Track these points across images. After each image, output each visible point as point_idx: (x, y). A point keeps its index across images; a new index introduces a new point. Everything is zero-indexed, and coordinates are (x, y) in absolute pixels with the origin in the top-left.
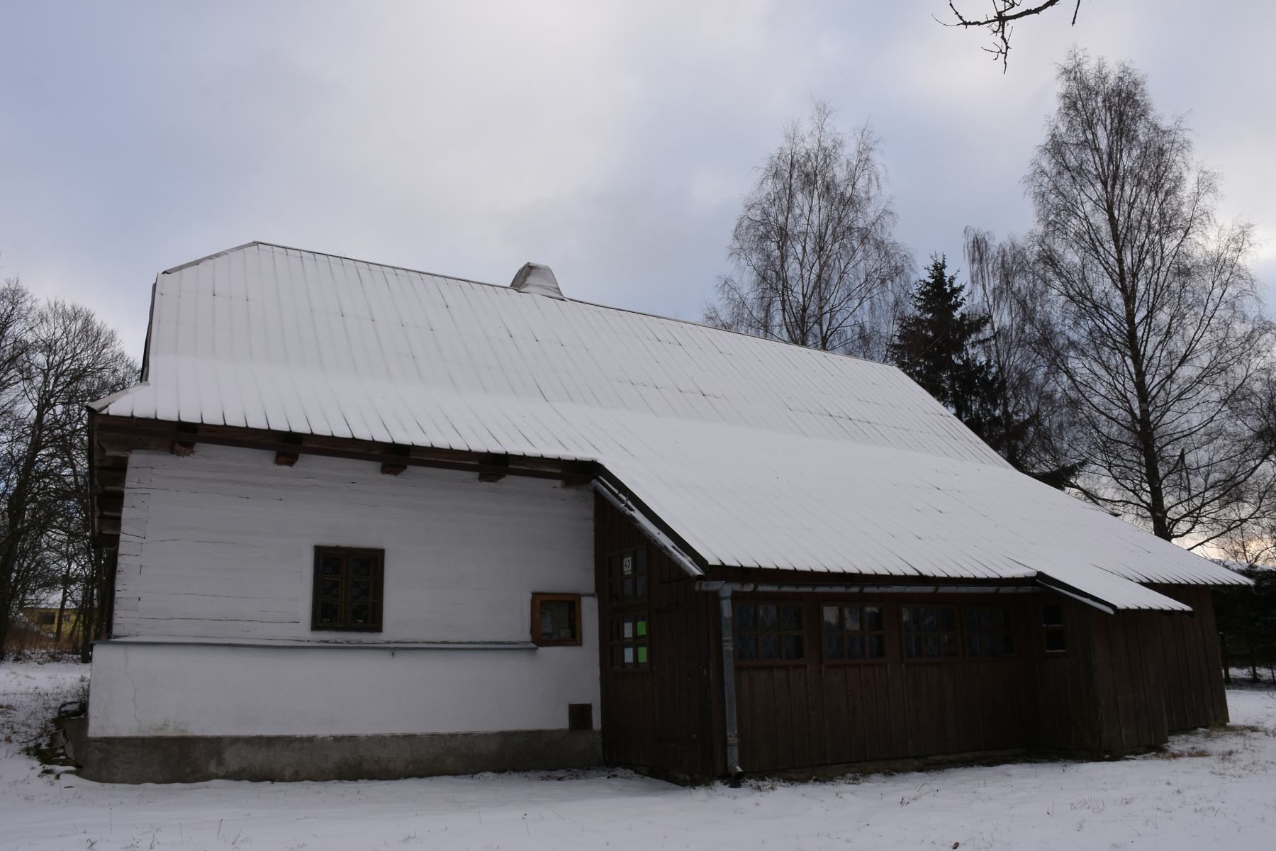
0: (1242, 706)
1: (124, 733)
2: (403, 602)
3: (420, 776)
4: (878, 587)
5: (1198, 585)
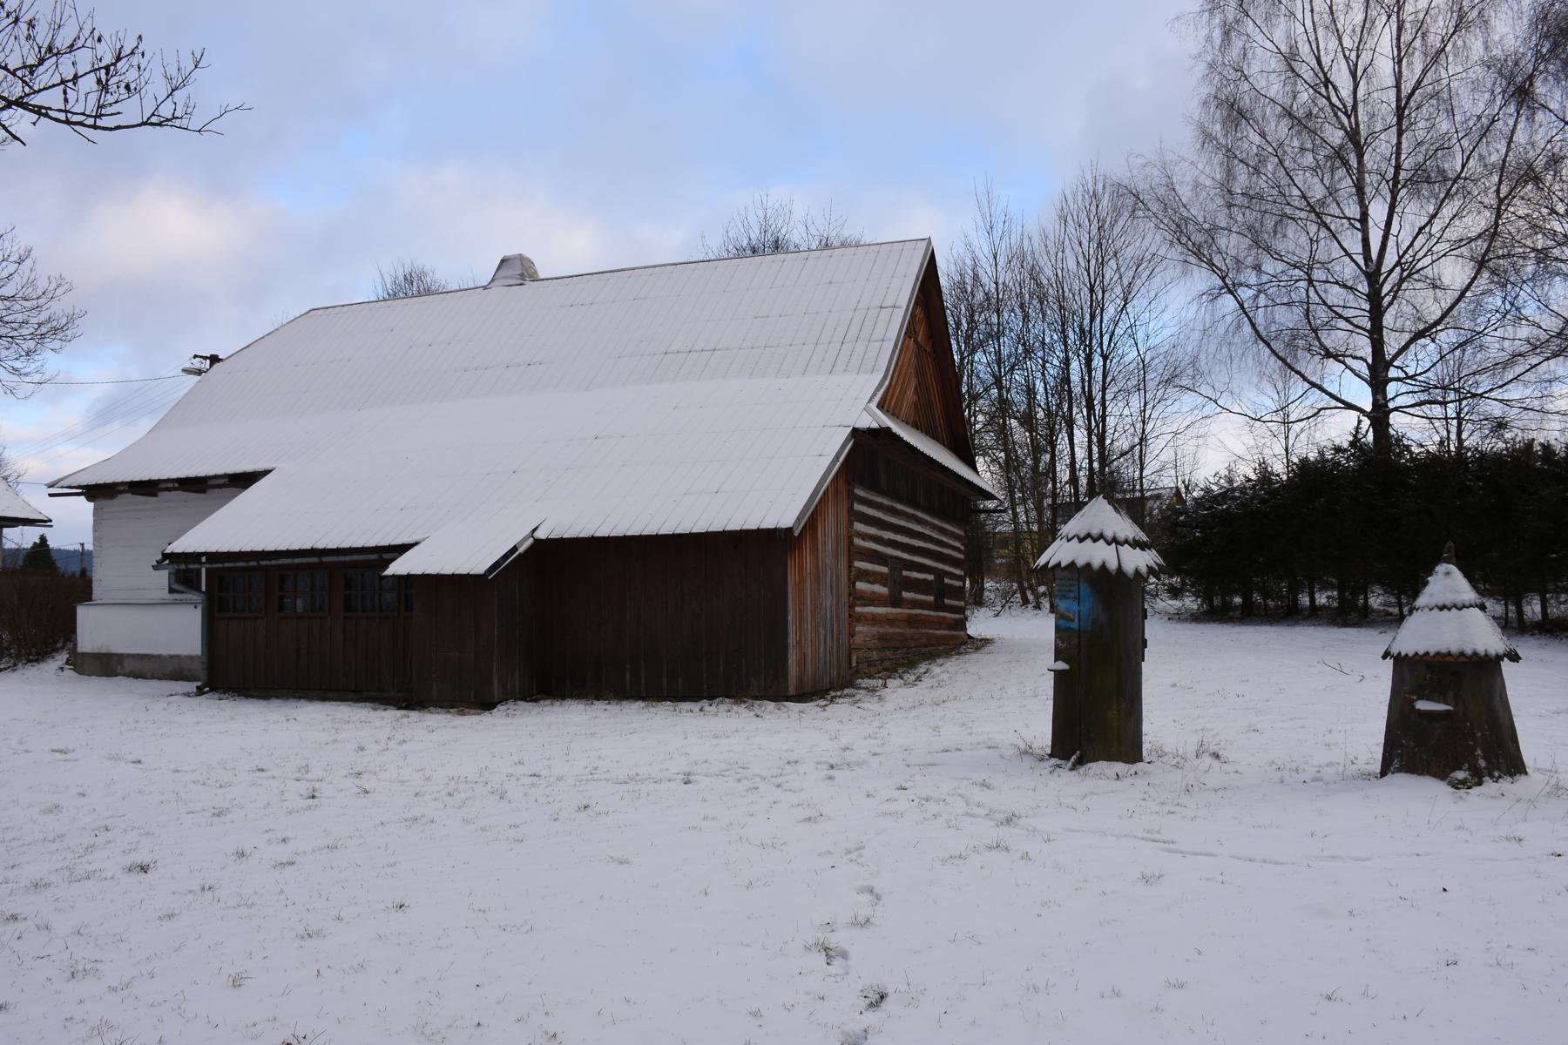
0: (979, 624)
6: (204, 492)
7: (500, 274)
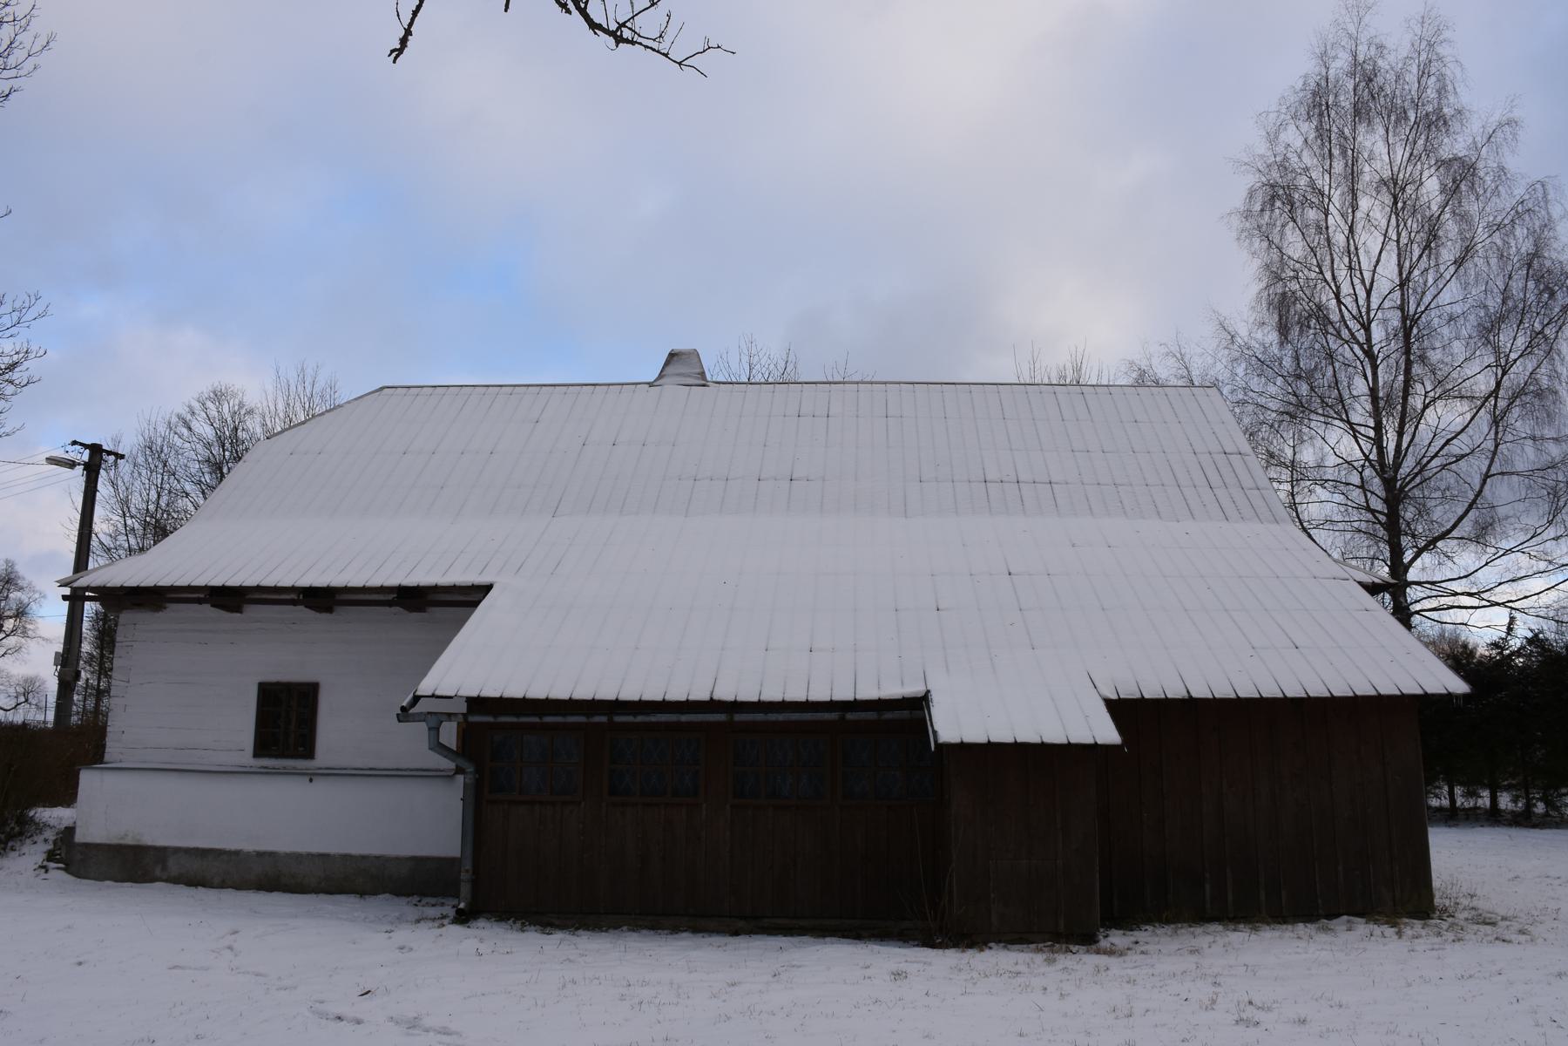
0: (1458, 858)
1: (98, 841)
2: (336, 731)
3: (362, 893)
4: (635, 715)
5: (1380, 698)
6: (329, 610)
7: (669, 370)
